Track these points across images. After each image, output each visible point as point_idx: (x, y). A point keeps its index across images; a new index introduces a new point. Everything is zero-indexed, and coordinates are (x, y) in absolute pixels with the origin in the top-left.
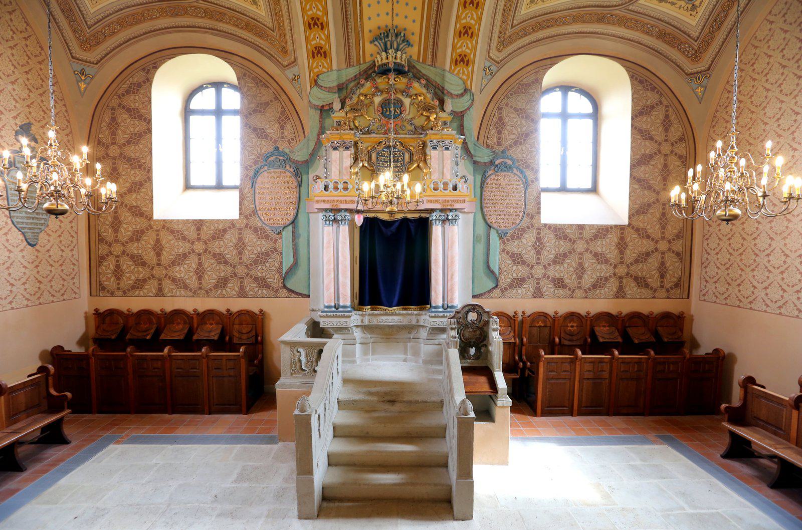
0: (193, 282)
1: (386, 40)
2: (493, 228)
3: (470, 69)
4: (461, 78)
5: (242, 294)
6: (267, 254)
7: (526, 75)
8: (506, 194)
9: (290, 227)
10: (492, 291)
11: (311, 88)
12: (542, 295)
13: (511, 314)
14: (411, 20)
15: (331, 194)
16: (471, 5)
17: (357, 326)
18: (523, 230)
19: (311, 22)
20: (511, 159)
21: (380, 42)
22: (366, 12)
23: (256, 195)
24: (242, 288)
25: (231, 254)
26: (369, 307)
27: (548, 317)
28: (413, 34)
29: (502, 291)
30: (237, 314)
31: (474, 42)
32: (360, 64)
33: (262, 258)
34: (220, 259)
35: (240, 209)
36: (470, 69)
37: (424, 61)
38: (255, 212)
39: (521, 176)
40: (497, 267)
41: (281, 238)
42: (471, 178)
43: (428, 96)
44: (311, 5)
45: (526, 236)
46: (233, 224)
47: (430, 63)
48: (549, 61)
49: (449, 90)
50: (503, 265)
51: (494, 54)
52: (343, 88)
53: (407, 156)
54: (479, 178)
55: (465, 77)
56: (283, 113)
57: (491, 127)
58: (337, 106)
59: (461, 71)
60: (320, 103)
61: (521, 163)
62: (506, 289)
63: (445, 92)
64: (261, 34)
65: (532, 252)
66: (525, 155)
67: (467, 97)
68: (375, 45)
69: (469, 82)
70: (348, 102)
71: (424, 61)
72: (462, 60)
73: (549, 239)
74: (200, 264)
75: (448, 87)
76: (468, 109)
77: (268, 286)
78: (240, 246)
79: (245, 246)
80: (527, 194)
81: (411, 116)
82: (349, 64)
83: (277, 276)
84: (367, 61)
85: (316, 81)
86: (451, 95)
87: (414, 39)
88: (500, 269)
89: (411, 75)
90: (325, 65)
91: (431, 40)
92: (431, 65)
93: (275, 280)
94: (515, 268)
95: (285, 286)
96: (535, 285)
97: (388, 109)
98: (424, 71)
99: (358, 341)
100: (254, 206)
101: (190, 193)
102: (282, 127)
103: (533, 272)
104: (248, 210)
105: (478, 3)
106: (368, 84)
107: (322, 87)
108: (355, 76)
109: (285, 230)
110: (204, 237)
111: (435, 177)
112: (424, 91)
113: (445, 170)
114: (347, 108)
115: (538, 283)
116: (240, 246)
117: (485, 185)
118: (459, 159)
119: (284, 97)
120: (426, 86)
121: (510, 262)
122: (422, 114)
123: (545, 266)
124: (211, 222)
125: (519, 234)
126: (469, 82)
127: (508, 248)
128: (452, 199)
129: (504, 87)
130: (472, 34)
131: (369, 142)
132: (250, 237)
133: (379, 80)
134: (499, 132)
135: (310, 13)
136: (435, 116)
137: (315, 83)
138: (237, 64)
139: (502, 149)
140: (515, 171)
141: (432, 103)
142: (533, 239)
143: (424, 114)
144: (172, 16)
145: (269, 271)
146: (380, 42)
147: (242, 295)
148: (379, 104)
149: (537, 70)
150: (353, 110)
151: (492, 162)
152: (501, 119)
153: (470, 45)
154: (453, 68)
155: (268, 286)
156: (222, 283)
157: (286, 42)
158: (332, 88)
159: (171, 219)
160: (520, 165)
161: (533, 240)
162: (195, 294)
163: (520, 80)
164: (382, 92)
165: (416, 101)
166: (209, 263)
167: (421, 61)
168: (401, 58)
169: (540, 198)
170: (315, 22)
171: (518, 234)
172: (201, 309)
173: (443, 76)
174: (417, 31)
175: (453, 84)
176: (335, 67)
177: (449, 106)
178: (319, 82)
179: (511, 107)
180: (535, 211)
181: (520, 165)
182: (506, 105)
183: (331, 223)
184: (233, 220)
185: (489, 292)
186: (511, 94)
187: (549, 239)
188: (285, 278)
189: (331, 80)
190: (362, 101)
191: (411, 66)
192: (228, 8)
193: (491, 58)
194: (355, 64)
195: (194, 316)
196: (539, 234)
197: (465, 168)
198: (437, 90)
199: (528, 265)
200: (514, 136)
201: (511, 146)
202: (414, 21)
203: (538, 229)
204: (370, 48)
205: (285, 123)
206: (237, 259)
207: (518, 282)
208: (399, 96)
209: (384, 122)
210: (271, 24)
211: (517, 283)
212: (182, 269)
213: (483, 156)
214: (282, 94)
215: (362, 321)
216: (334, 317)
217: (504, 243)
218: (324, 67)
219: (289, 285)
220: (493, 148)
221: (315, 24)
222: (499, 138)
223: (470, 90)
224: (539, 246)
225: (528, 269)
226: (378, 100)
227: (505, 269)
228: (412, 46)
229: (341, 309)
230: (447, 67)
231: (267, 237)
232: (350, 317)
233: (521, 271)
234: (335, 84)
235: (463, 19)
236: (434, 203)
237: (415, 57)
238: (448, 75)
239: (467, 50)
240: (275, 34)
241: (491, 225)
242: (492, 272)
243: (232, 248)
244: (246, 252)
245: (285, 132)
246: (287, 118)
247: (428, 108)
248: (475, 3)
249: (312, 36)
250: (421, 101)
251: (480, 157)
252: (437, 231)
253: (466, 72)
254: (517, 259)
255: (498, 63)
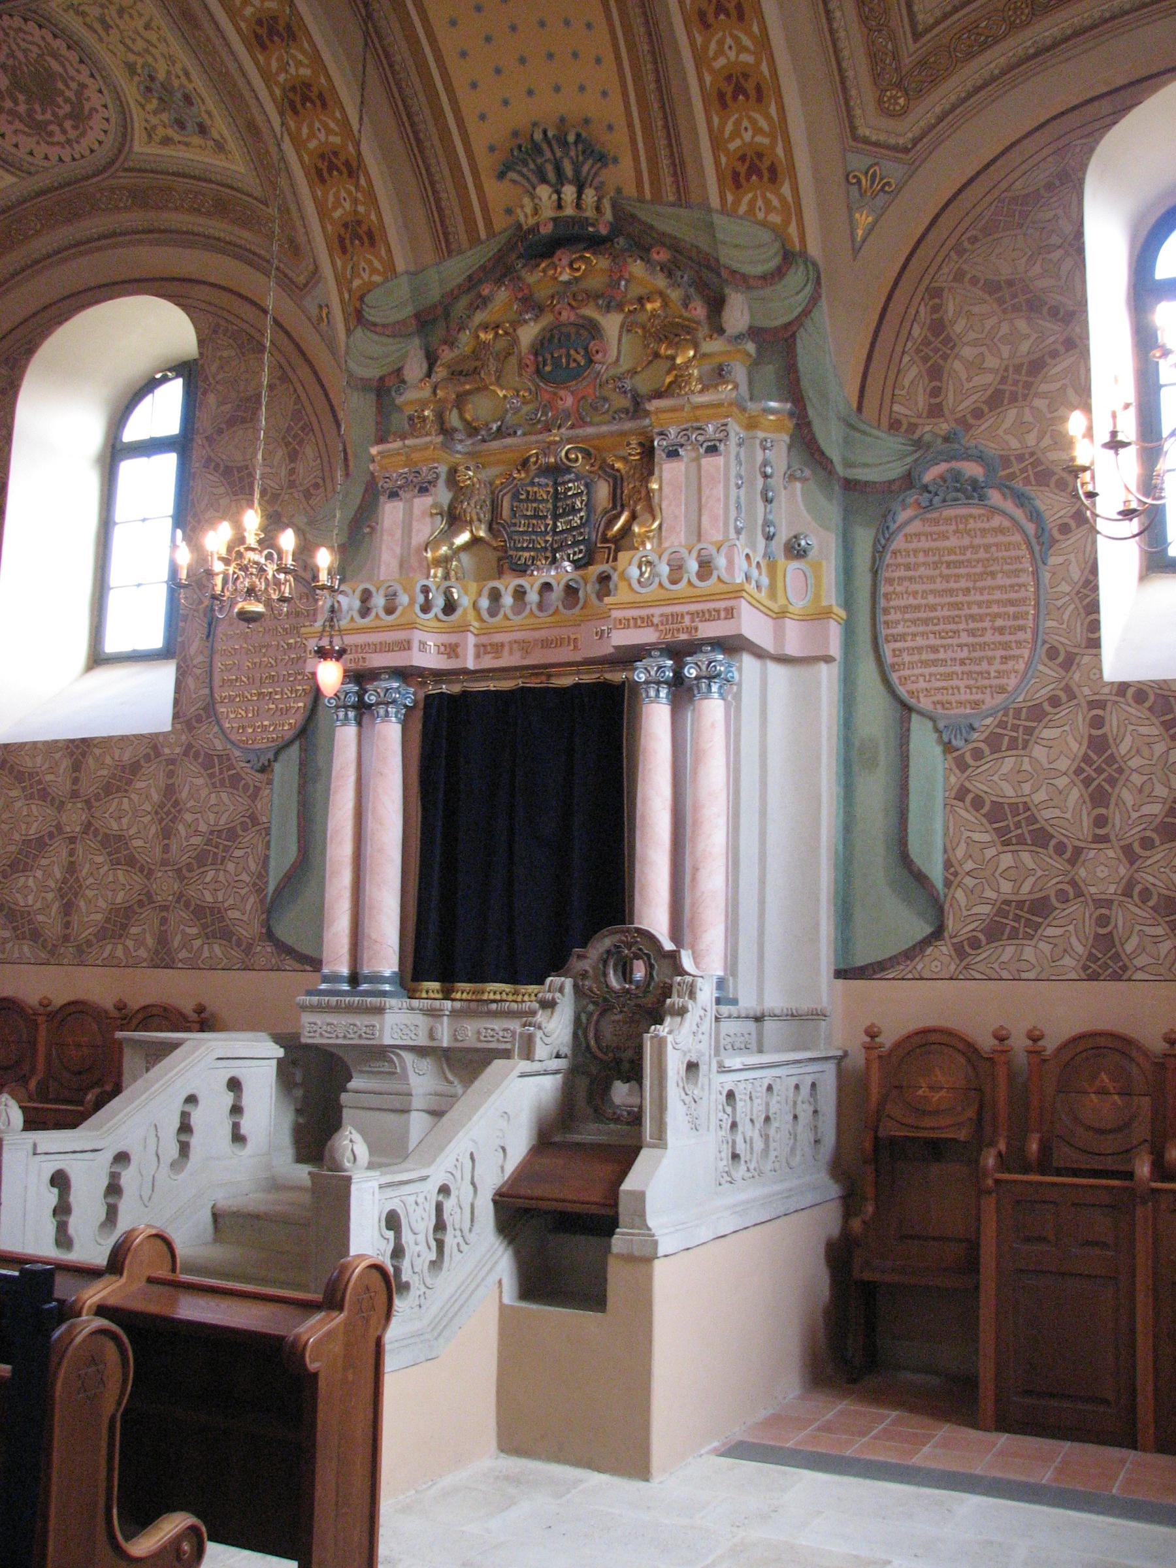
0: (50, 921)
1: (539, 161)
2: (921, 713)
3: (786, 189)
4: (764, 224)
5: (163, 958)
6: (232, 835)
7: (1024, 167)
8: (963, 584)
9: (294, 751)
10: (922, 951)
11: (349, 332)
12: (1124, 968)
13: (986, 1043)
14: (588, 88)
15: (378, 623)
16: (722, 17)
17: (420, 1051)
18: (1037, 713)
19: (320, 165)
20: (980, 458)
21: (525, 170)
22: (470, 104)
23: (217, 657)
24: (163, 940)
25: (143, 839)
26: (436, 985)
27: (1134, 1054)
28: (610, 128)
29: (960, 952)
30: (140, 1016)
31: (773, 110)
32: (479, 241)
33: (216, 848)
34: (116, 847)
35: (176, 702)
36: (786, 189)
37: (657, 197)
38: (209, 709)
39: (1018, 514)
40: (938, 859)
41: (270, 782)
42: (824, 543)
43: (675, 295)
44: (311, 127)
45: (1047, 733)
46: (155, 748)
47: (672, 198)
48: (1105, 106)
49: (735, 266)
50: (960, 852)
51: (871, 124)
52: (435, 320)
53: (603, 490)
54: (864, 539)
55: (775, 218)
56: (297, 415)
57: (906, 359)
58: (414, 369)
59: (760, 203)
60: (372, 372)
61: (1016, 467)
62: (975, 944)
63: (725, 274)
64: (247, 221)
65: (1075, 794)
66: (1031, 440)
67: (796, 277)
68: (514, 182)
69: (793, 230)
70: (447, 355)
71: (657, 197)
72: (755, 169)
73: (1133, 735)
74: (71, 868)
75: (730, 257)
76: (806, 313)
77: (227, 935)
78: (169, 809)
79: (179, 811)
80: (1046, 576)
81: (625, 365)
82: (446, 246)
83: (252, 900)
84: (497, 227)
85: (359, 313)
86: (744, 281)
87: (617, 142)
88: (948, 864)
89: (621, 242)
90: (377, 264)
91: (660, 134)
92: (678, 204)
93: (244, 916)
94: (1007, 860)
95: (270, 935)
96: (1090, 928)
97: (548, 356)
98: (663, 226)
99: (417, 1102)
100: (207, 691)
101: (103, 675)
102: (293, 456)
103: (1082, 872)
104: (192, 709)
105: (739, 7)
106: (502, 295)
107: (375, 325)
108: (470, 278)
109: (280, 758)
110: (88, 788)
111: (677, 539)
112: (661, 282)
113: (705, 519)
114: (440, 373)
115: (1103, 921)
116: (169, 809)
117: (888, 559)
118: (777, 481)
119: (304, 372)
120: (668, 270)
121: (986, 837)
122: (657, 355)
123: (1128, 851)
124: (106, 743)
125: (1018, 728)
126: (793, 230)
127: (978, 786)
128: (693, 608)
129: (947, 221)
130: (759, 89)
131: (498, 463)
132: (193, 782)
133: (532, 278)
134: (935, 373)
135: (312, 145)
136: (691, 353)
137: (357, 318)
138: (203, 306)
139: (944, 427)
140: (994, 497)
141: (686, 314)
142: (1074, 746)
143: (662, 351)
144: (68, 221)
145: (231, 889)
146: (525, 170)
147: (163, 960)
148: (533, 345)
149: (1061, 144)
150: (456, 374)
151: (909, 480)
152: (938, 327)
153: (763, 124)
154: (730, 198)
155: (227, 935)
156: (118, 922)
157: (294, 228)
158: (403, 322)
159: (21, 741)
160: (1012, 476)
161: (1077, 748)
162: (52, 954)
163: (1004, 185)
164: (539, 309)
165: (642, 318)
166: (94, 861)
167: (648, 196)
168: (592, 207)
169: (1096, 588)
170: (331, 162)
171: (1015, 728)
172: (60, 999)
173: (711, 226)
174: (621, 123)
175: (742, 243)
176: (400, 266)
177: (738, 314)
178: (370, 315)
179: (974, 281)
180: (1079, 633)
181: (1012, 476)
182: (955, 279)
183: (351, 714)
184: (157, 735)
185: (910, 954)
186: (974, 240)
187: (1133, 735)
188: (271, 908)
189: (393, 303)
190: (485, 345)
191: (623, 220)
192: (173, 174)
193: (866, 141)
194: (465, 245)
195: (40, 1019)
196: (1097, 723)
197: (800, 509)
198: (706, 274)
199: (1060, 849)
200: (989, 378)
201: (978, 414)
202: (604, 94)
203: (1092, 705)
204: (498, 192)
205: (300, 443)
206: (158, 850)
207: (1023, 917)
208: (589, 311)
209: (546, 396)
210: (259, 188)
211: (1017, 918)
212: (31, 882)
213: (881, 459)
214: (297, 360)
215: (432, 1036)
216: (350, 1009)
217: (962, 765)
218: (374, 271)
219: (281, 932)
220: (912, 427)
221: (332, 167)
222: (935, 392)
223: (803, 253)
224: (1099, 769)
225: (1059, 864)
226: (528, 334)
227: (969, 865)
228: (615, 161)
229: (364, 987)
230: (715, 202)
231: (235, 780)
232: (380, 1010)
233: (1032, 871)
234: (409, 310)
235: (715, 59)
236: (636, 626)
237: (630, 190)
238: (719, 220)
239: (759, 139)
240: (270, 210)
241: (912, 702)
242: (920, 878)
243: (149, 818)
244: (181, 827)
245: (301, 468)
246: (307, 428)
247: (674, 332)
248: (731, 6)
249: (331, 199)
250: (653, 315)
251: (866, 465)
252: (657, 718)
253: (776, 202)
254: (1014, 824)
255: (906, 150)
